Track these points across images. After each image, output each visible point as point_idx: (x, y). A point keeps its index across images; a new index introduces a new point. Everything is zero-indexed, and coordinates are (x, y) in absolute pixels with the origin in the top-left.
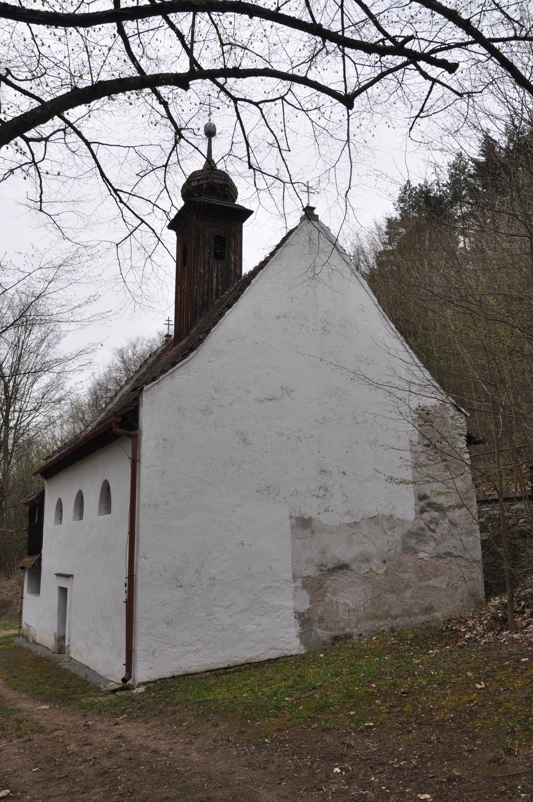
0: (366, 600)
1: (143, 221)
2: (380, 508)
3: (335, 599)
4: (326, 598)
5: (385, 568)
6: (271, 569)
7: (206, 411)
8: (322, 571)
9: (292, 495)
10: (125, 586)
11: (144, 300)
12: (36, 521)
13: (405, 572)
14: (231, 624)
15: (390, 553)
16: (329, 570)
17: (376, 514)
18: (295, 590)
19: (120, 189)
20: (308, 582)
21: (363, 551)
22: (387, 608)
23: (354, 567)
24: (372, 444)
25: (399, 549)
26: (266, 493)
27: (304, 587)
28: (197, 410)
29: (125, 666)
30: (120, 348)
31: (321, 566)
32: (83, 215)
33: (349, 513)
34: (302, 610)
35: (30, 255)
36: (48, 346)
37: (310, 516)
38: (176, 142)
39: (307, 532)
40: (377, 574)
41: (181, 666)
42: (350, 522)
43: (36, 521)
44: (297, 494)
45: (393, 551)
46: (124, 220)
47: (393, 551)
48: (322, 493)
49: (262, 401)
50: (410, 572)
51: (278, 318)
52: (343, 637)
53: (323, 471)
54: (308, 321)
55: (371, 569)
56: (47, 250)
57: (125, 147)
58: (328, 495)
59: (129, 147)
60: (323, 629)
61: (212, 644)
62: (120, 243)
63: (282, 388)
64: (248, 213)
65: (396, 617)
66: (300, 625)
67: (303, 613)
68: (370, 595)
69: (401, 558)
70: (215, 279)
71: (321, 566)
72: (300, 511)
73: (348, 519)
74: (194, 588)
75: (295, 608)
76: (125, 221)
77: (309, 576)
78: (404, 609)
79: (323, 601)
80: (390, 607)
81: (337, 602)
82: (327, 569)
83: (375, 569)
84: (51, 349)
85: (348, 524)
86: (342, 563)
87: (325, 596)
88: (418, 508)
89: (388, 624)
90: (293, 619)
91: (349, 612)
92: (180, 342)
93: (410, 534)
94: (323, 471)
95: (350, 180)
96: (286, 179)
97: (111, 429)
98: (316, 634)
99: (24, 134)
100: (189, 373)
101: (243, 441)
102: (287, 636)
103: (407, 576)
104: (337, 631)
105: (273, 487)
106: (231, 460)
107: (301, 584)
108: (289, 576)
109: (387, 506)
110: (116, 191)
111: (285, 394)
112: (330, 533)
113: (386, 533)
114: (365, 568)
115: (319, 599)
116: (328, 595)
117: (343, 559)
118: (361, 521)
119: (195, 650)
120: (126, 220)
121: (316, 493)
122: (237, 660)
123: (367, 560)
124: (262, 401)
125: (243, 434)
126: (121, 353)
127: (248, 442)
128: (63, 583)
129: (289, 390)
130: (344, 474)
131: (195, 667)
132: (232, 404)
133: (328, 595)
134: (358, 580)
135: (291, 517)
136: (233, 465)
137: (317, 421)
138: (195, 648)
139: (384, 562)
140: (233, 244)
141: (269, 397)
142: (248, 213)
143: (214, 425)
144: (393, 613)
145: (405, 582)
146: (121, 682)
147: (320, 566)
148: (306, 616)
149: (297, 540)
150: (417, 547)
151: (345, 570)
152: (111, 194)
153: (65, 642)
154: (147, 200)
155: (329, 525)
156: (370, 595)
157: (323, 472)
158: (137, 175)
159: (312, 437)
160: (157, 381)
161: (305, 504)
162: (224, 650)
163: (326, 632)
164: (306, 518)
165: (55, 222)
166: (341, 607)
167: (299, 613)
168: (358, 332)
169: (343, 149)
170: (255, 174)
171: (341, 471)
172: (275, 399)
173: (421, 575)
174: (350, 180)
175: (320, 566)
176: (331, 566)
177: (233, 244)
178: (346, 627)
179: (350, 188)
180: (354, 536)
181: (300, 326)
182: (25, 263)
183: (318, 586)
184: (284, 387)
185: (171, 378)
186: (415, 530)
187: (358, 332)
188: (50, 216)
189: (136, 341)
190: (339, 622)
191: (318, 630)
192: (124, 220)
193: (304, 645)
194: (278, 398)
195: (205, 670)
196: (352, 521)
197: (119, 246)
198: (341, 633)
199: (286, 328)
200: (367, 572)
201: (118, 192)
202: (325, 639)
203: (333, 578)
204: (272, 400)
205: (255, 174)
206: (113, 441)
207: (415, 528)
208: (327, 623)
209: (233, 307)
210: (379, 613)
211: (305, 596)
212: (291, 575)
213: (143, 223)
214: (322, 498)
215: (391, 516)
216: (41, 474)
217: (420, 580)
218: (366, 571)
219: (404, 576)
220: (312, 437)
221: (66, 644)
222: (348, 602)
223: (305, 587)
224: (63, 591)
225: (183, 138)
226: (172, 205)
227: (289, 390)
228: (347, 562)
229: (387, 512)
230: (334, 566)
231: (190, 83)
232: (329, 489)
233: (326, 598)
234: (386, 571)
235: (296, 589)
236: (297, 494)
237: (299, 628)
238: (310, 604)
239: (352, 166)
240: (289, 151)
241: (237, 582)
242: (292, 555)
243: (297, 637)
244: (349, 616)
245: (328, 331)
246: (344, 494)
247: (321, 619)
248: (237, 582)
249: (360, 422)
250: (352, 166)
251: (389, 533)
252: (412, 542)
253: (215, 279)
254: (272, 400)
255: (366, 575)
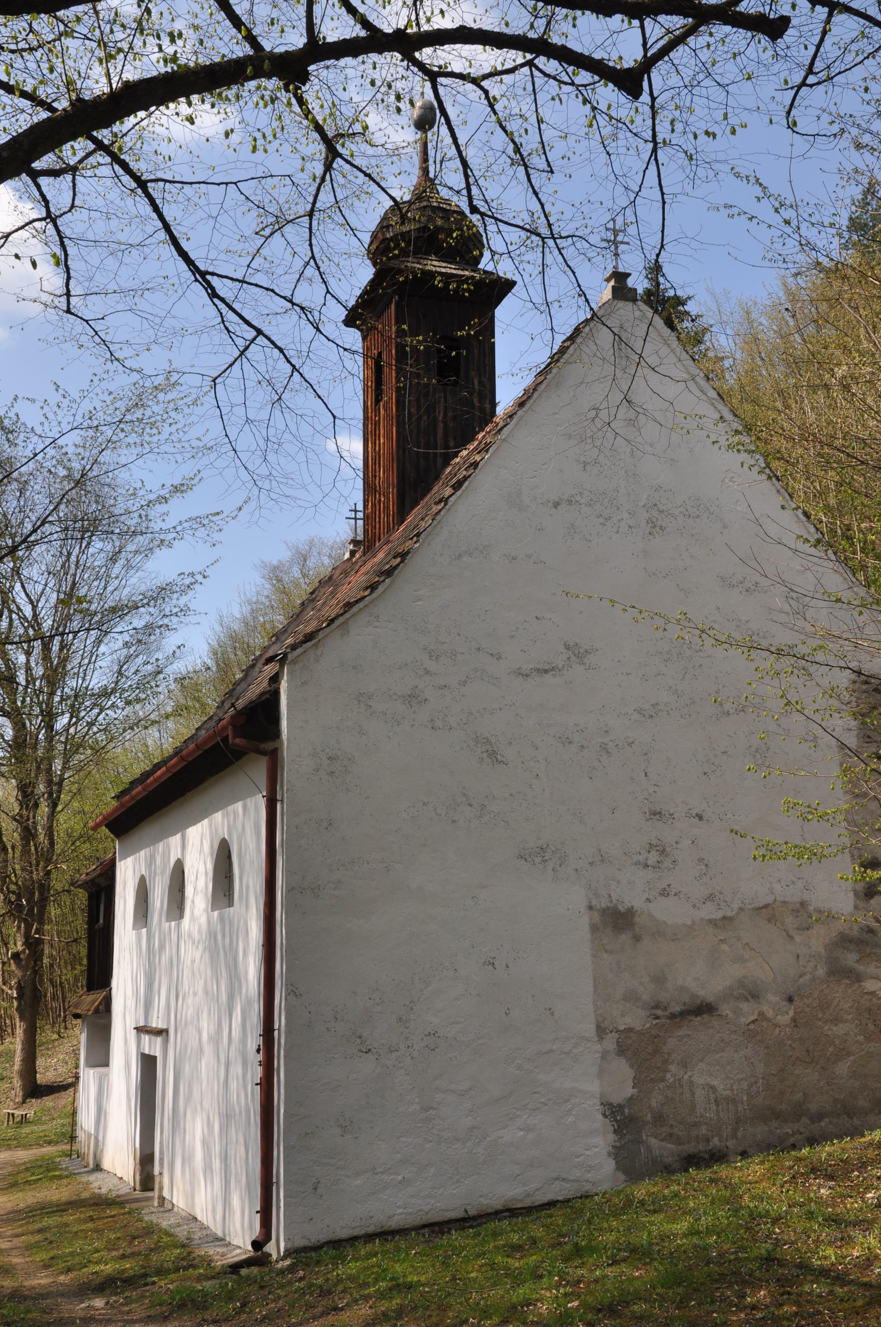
0: (753, 1080)
1: (259, 332)
2: (777, 887)
3: (686, 1077)
4: (668, 1076)
5: (791, 1013)
6: (552, 1014)
7: (413, 698)
8: (657, 1018)
9: (591, 864)
10: (258, 1051)
11: (274, 484)
12: (101, 921)
13: (836, 1021)
14: (472, 1128)
15: (801, 980)
16: (673, 1016)
17: (770, 899)
18: (602, 1058)
19: (210, 270)
20: (630, 1042)
21: (744, 977)
22: (799, 1096)
23: (726, 1009)
24: (758, 756)
25: (821, 972)
26: (538, 860)
27: (621, 1050)
28: (395, 697)
29: (259, 1215)
30: (275, 563)
31: (656, 1007)
32: (151, 317)
33: (711, 897)
34: (617, 1098)
35: (53, 402)
36: (128, 566)
37: (630, 905)
38: (328, 167)
39: (625, 938)
40: (776, 1025)
41: (371, 1214)
42: (713, 916)
43: (101, 921)
44: (602, 861)
45: (808, 977)
46: (227, 329)
47: (808, 977)
48: (653, 858)
49: (527, 675)
50: (846, 1021)
51: (556, 505)
52: (707, 1156)
53: (656, 814)
54: (618, 509)
55: (761, 1014)
56: (86, 393)
57: (219, 184)
58: (667, 863)
59: (227, 184)
60: (662, 1140)
61: (432, 1170)
62: (219, 376)
63: (568, 647)
64: (504, 287)
65: (820, 1116)
66: (615, 1131)
67: (620, 1106)
68: (760, 1069)
69: (826, 992)
70: (441, 426)
71: (656, 1007)
72: (610, 896)
73: (709, 912)
74: (395, 1054)
75: (602, 1095)
76: (229, 331)
77: (630, 1030)
78: (836, 1100)
79: (663, 1080)
80: (805, 1095)
81: (691, 1082)
82: (667, 1013)
83: (770, 1013)
84: (133, 571)
85: (710, 921)
86: (699, 1002)
87: (667, 1071)
88: (860, 887)
89: (802, 1130)
90: (600, 1117)
91: (717, 1105)
92: (374, 556)
93: (845, 941)
94: (656, 814)
95: (663, 232)
96: (544, 231)
97: (225, 739)
98: (649, 1149)
99: (33, 165)
100: (377, 624)
101: (489, 756)
102: (588, 1153)
103: (839, 1030)
104: (693, 1144)
105: (553, 848)
106: (465, 795)
107: (615, 1046)
108: (589, 1029)
109: (793, 883)
110: (203, 274)
111: (573, 659)
112: (673, 940)
113: (791, 937)
114: (749, 1011)
115: (652, 1076)
116: (673, 1068)
117: (702, 993)
118: (737, 914)
119: (400, 1182)
120: (230, 329)
121: (641, 858)
122: (485, 1202)
123: (753, 994)
124: (527, 675)
125: (488, 742)
126: (275, 574)
127: (499, 757)
128: (152, 1046)
129: (582, 651)
130: (700, 817)
131: (399, 1217)
132: (465, 682)
133: (673, 1068)
134: (734, 1037)
135: (591, 908)
136: (470, 805)
137: (640, 711)
138: (400, 1178)
139: (790, 1000)
140: (476, 351)
141: (541, 666)
142: (504, 287)
143: (430, 725)
144: (813, 1107)
145: (837, 1042)
146: (250, 1248)
147: (653, 1008)
148: (627, 1111)
149: (605, 955)
150: (860, 968)
151: (705, 1016)
152: (196, 280)
153: (153, 1166)
154: (267, 289)
155: (669, 923)
156: (760, 1069)
157: (655, 814)
158: (257, 233)
159: (630, 744)
160: (313, 642)
161: (619, 882)
162: (458, 1182)
163: (670, 1146)
164: (622, 910)
165: (97, 334)
166: (700, 1094)
167: (611, 1104)
168: (725, 527)
169: (647, 168)
170: (484, 223)
171: (694, 812)
172: (553, 669)
173: (871, 1027)
174: (663, 232)
175: (653, 1008)
176: (677, 1008)
177: (476, 351)
178: (713, 1137)
179: (662, 246)
180: (725, 947)
181: (601, 520)
182: (43, 419)
183: (650, 1049)
184: (572, 644)
185: (342, 635)
186: (855, 932)
187: (725, 527)
188: (87, 321)
189: (307, 547)
190: (696, 1125)
191: (653, 1141)
192: (227, 329)
193: (625, 1172)
194: (560, 666)
195: (421, 1223)
196: (719, 915)
197: (217, 381)
198: (701, 1147)
199: (572, 525)
200: (754, 1022)
201: (208, 277)
202: (668, 1160)
203: (681, 1033)
204: (546, 671)
205: (484, 223)
206: (232, 763)
207: (856, 928)
208: (671, 1126)
209: (463, 487)
210: (784, 1106)
211: (623, 1070)
212: (592, 1027)
213: (260, 338)
214: (654, 867)
215: (803, 904)
216: (107, 826)
217: (868, 1039)
218: (752, 1018)
219: (834, 1028)
220: (630, 744)
221: (156, 1171)
222: (715, 1083)
223: (622, 1052)
224: (148, 1064)
225: (340, 155)
226: (328, 292)
227: (582, 651)
228: (711, 999)
229: (793, 894)
230: (683, 1008)
231: (311, 68)
232: (668, 849)
233: (668, 1076)
234: (794, 1020)
235: (604, 1056)
236: (602, 861)
237: (612, 1137)
238: (633, 1088)
239: (664, 203)
240: (552, 172)
241: (481, 1041)
242: (595, 986)
243: (609, 1155)
244: (718, 1112)
245: (661, 528)
246: (701, 860)
247: (659, 1118)
248: (481, 1041)
249: (732, 711)
250: (664, 203)
251: (798, 939)
252: (850, 958)
253: (441, 426)
254: (546, 671)
255: (752, 1027)
